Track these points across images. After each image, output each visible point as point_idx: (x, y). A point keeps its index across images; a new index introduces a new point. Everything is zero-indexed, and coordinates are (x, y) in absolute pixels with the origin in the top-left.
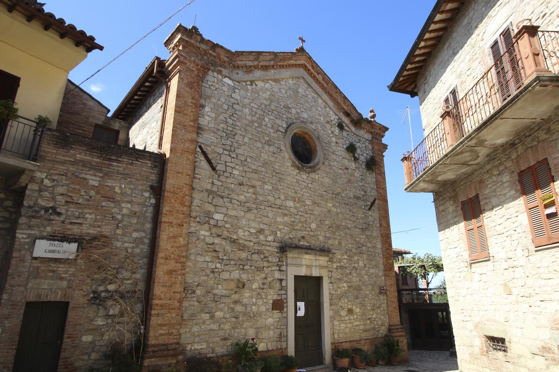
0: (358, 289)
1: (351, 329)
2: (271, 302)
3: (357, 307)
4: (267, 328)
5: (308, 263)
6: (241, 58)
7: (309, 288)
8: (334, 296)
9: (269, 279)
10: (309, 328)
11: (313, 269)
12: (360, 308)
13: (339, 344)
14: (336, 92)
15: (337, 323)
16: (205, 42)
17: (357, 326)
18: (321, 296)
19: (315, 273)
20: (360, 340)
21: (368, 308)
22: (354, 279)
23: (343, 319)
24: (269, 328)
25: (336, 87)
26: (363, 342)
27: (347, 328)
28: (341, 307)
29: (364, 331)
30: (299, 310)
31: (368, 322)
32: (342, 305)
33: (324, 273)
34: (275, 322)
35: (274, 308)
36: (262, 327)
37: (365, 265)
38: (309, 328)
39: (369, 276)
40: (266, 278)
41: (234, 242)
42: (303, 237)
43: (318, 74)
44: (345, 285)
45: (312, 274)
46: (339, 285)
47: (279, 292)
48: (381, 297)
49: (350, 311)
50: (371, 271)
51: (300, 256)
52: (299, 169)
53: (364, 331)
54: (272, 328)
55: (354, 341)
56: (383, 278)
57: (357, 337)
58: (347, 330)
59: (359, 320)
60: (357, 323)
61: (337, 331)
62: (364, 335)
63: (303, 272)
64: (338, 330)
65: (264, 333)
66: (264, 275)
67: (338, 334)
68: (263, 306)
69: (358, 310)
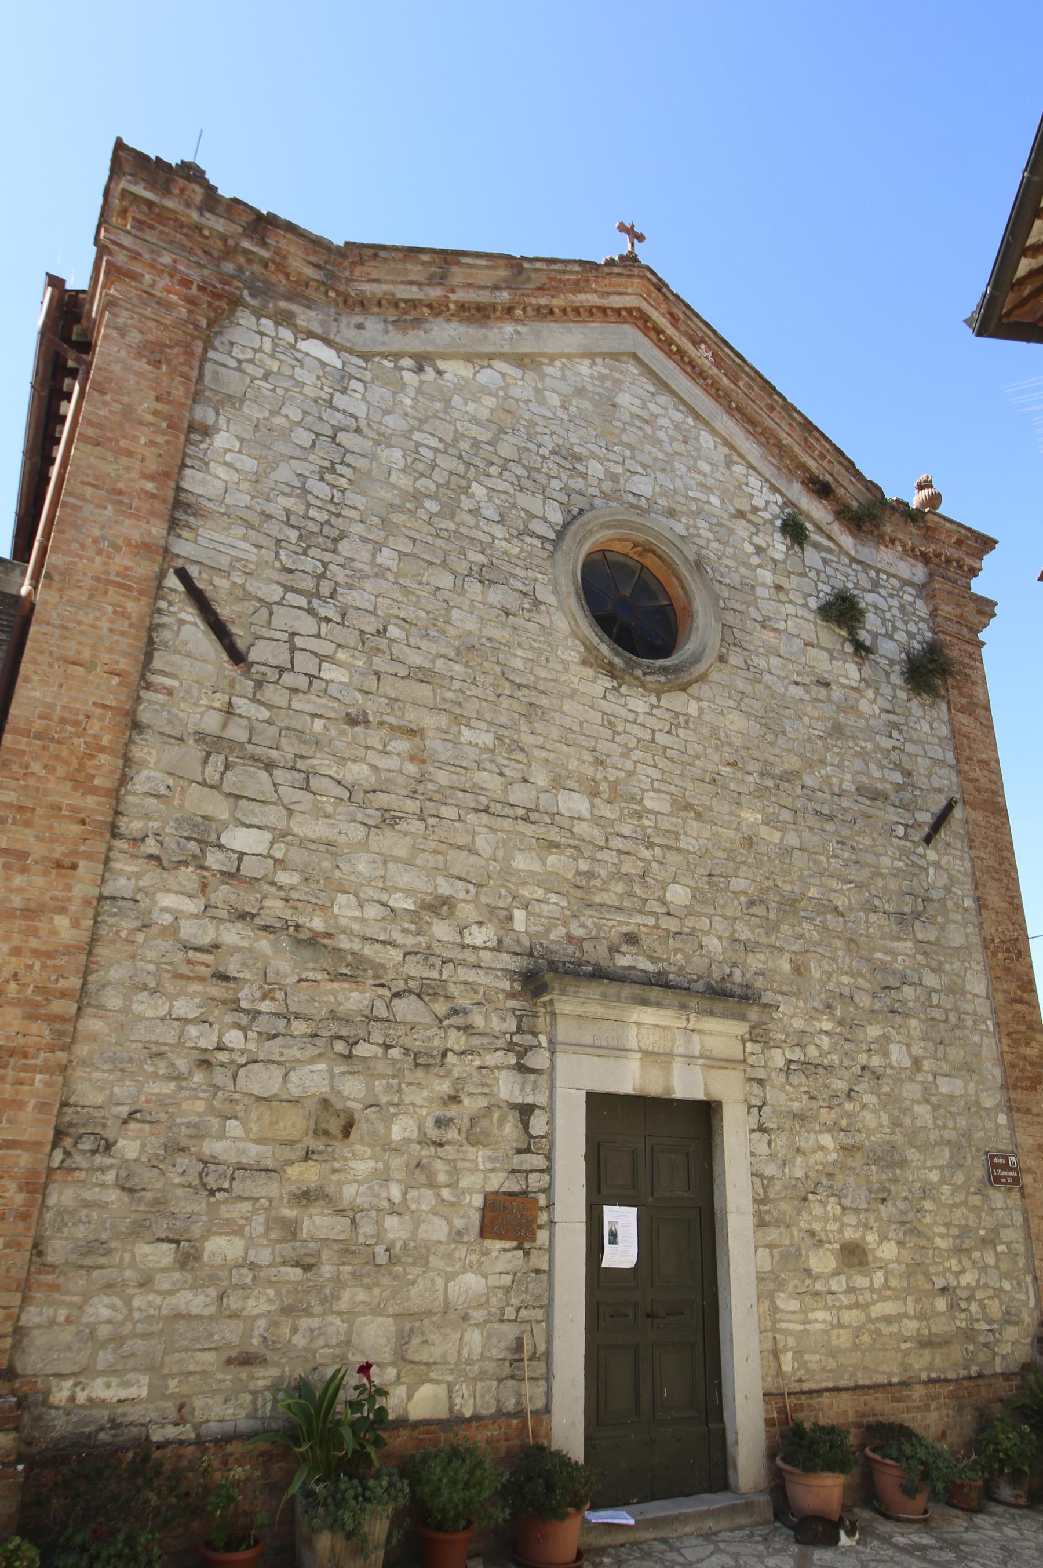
0: (889, 1158)
1: (858, 1331)
2: (478, 1201)
3: (884, 1238)
5: (651, 1041)
6: (371, 269)
7: (659, 1150)
8: (778, 1186)
11: (678, 1067)
12: (901, 1244)
14: (772, 408)
15: (794, 1305)
17: (888, 1319)
19: (686, 1085)
20: (903, 1384)
21: (939, 1242)
22: (869, 1119)
23: (819, 1286)
24: (465, 1318)
25: (769, 388)
27: (840, 1326)
28: (812, 1234)
31: (941, 1304)
32: (817, 1227)
37: (917, 1063)
39: (936, 1108)
43: (695, 344)
44: (826, 1140)
47: (517, 1159)
48: (998, 1197)
49: (853, 1255)
50: (945, 1086)
51: (613, 1014)
54: (478, 1315)
56: (1002, 1119)
57: (888, 1368)
58: (842, 1339)
59: (900, 1296)
61: (791, 1341)
62: (921, 1364)
63: (627, 1078)
64: (800, 1336)
67: (798, 1353)
68: (437, 1217)
69: (888, 1251)
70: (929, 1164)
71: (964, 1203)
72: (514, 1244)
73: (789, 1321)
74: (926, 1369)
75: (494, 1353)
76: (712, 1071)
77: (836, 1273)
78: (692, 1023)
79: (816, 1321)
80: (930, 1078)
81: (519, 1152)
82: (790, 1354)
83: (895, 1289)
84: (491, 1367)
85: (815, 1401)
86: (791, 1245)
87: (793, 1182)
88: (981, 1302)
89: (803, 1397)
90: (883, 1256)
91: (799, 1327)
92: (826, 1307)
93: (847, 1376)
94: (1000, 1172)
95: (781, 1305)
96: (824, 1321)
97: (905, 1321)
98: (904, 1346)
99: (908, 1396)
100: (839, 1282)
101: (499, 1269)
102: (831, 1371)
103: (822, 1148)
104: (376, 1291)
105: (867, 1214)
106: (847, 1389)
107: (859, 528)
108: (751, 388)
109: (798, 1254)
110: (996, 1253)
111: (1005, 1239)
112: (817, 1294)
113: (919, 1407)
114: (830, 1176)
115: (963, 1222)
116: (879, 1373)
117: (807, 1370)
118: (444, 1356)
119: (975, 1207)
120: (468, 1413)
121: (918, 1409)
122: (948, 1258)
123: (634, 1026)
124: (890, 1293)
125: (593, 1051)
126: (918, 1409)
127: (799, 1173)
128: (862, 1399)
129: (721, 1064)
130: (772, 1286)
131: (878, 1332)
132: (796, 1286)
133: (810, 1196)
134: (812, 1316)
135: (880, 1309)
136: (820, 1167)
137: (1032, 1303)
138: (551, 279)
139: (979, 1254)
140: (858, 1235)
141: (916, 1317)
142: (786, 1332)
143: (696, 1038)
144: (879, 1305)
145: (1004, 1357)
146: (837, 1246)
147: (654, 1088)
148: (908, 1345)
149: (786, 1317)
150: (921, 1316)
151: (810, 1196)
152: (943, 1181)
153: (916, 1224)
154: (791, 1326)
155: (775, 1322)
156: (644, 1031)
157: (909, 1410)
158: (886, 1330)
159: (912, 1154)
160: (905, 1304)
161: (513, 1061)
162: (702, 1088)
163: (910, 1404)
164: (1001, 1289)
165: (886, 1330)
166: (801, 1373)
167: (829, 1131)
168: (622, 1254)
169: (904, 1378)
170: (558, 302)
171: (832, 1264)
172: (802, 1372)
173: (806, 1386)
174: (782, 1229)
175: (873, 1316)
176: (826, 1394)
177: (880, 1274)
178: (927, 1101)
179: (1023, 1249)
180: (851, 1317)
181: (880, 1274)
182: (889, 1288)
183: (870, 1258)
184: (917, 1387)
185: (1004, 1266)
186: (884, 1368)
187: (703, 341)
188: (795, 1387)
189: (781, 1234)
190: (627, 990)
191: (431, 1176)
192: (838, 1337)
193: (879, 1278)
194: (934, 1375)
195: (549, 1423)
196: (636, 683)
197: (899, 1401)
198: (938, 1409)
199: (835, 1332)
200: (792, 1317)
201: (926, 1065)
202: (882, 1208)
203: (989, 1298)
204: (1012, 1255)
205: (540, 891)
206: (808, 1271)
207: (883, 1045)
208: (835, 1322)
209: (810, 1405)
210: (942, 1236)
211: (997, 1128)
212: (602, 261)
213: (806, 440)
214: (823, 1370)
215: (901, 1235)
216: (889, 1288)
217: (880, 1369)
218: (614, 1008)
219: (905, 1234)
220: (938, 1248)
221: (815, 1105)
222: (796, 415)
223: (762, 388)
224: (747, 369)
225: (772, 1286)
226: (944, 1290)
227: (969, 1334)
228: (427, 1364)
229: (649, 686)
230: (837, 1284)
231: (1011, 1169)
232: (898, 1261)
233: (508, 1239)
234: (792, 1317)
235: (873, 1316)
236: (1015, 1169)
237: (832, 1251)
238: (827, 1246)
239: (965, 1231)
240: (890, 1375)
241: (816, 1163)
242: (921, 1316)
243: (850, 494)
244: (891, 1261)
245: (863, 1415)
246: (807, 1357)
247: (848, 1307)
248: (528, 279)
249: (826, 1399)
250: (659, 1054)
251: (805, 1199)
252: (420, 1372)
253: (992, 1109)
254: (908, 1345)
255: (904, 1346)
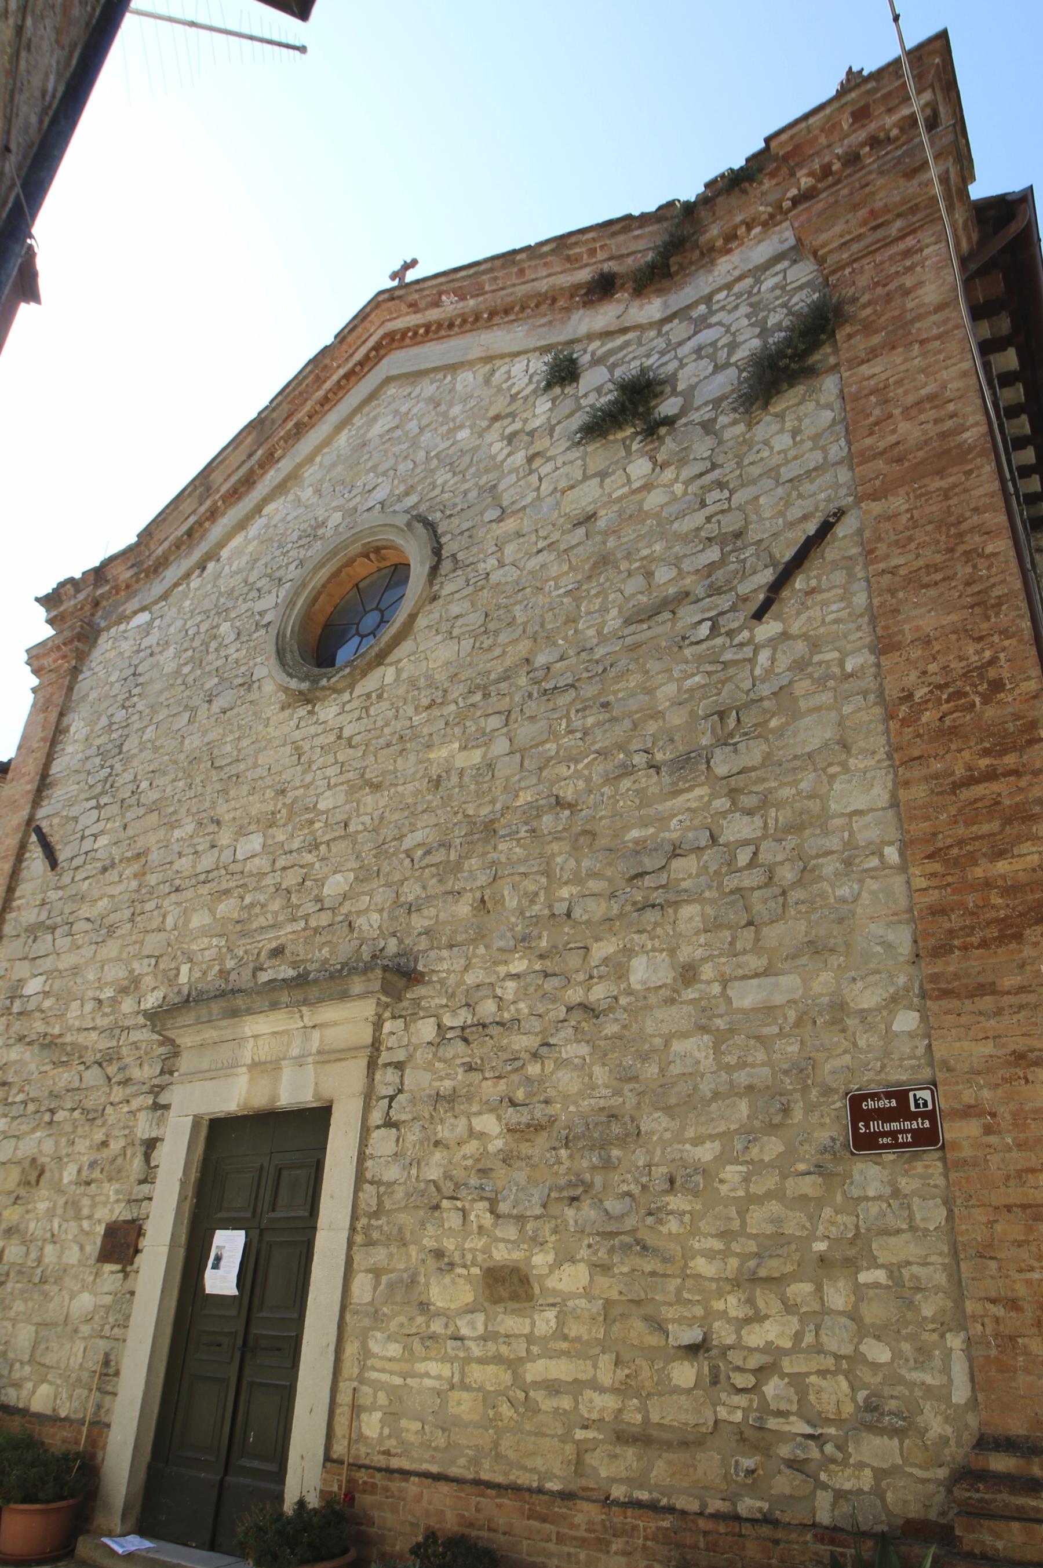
0: (608, 1133)
1: (489, 1400)
2: (101, 1229)
3: (565, 1257)
4: (69, 1328)
5: (265, 1051)
6: (159, 535)
7: (260, 1167)
8: (400, 1193)
9: (115, 1146)
10: (229, 1360)
11: (287, 1072)
12: (602, 1268)
13: (378, 1479)
14: (522, 272)
15: (394, 1349)
16: (82, 585)
17: (553, 1387)
18: (194, 1176)
19: (293, 1091)
20: (567, 1496)
21: (701, 1265)
22: (567, 1081)
23: (437, 1326)
24: (76, 1331)
25: (508, 258)
26: (586, 1514)
27: (464, 1387)
28: (439, 1254)
29: (623, 1437)
30: (216, 1266)
31: (684, 1374)
32: (449, 1244)
33: (344, 1089)
34: (96, 1308)
35: (106, 1255)
36: (55, 1324)
37: (688, 974)
38: (229, 1360)
39: (720, 1039)
40: (104, 1144)
41: (49, 1044)
42: (277, 952)
43: (437, 304)
44: (488, 1123)
45: (274, 1097)
46: (443, 1132)
47: (137, 1188)
48: (870, 1175)
49: (508, 1286)
50: (747, 996)
51: (228, 1034)
52: (308, 701)
53: (623, 1437)
54: (85, 1329)
55: (515, 1489)
56: (906, 1021)
57: (547, 1465)
58: (463, 1405)
59: (579, 1350)
60: (561, 1370)
61: (382, 1398)
62: (613, 1469)
63: (235, 1095)
64: (393, 1392)
65: (54, 1345)
66: (99, 1136)
67: (391, 1416)
68: (76, 1246)
69: (572, 1279)
70: (690, 1133)
71: (777, 1194)
72: (118, 1267)
73: (383, 1371)
74: (629, 1481)
75: (89, 1365)
76: (327, 1067)
77: (470, 1310)
78: (306, 1019)
79: (427, 1375)
80: (716, 989)
81: (141, 1182)
82: (378, 1415)
83: (578, 1339)
84: (85, 1375)
85: (395, 1485)
86: (406, 1270)
87: (422, 1186)
88: (797, 1380)
89: (378, 1475)
90: (559, 1286)
91: (398, 1381)
92: (445, 1359)
93: (462, 1461)
94: (885, 1122)
95: (375, 1347)
96: (439, 1377)
97: (588, 1394)
98: (580, 1434)
99: (564, 1517)
100: (472, 1325)
101: (105, 1290)
102: (436, 1449)
103: (481, 1136)
104: (30, 1304)
105: (538, 1223)
106: (458, 1481)
107: (669, 275)
108: (496, 279)
109: (414, 1281)
110: (857, 1288)
111: (883, 1257)
112: (432, 1337)
113: (584, 1540)
114: (484, 1172)
115: (770, 1229)
116: (525, 1469)
117: (402, 1442)
118: (58, 1362)
119: (804, 1198)
120: (63, 1415)
121: (583, 1543)
122: (720, 1295)
123: (251, 1040)
124: (565, 1345)
125: (201, 1076)
126: (583, 1543)
127: (433, 1173)
128: (474, 1500)
129: (333, 1057)
130: (367, 1322)
131: (531, 1408)
132: (402, 1325)
133: (445, 1204)
134: (420, 1367)
135: (536, 1370)
136: (469, 1162)
137: (960, 1394)
138: (291, 402)
139: (807, 1288)
140: (516, 1255)
141: (614, 1391)
142: (377, 1386)
143: (316, 1034)
144: (541, 1363)
145: (840, 1495)
146: (475, 1271)
147: (259, 1101)
148: (590, 1434)
149: (379, 1364)
150: (623, 1390)
151: (445, 1204)
152: (723, 1159)
153: (644, 1234)
154: (384, 1377)
155: (363, 1369)
156: (260, 1042)
157: (560, 1539)
158: (547, 1404)
159: (655, 1123)
160: (595, 1366)
161: (151, 1102)
162: (313, 1086)
163: (565, 1530)
164: (857, 1358)
165: (547, 1404)
166: (391, 1444)
167: (491, 1111)
168: (221, 1280)
169: (573, 1487)
170: (301, 415)
171: (466, 1295)
172: (393, 1442)
173: (395, 1463)
174: (393, 1249)
175: (529, 1378)
176: (414, 1479)
177: (551, 1314)
178: (704, 1029)
179: (941, 1278)
180: (488, 1376)
181: (551, 1314)
182: (565, 1338)
183: (537, 1290)
184: (585, 1506)
185: (873, 1313)
186: (538, 1462)
187: (440, 294)
188: (380, 1461)
189: (391, 1256)
190: (216, 1007)
191: (78, 1210)
192: (459, 1403)
193: (546, 1321)
194: (644, 1496)
195: (107, 1437)
196: (328, 693)
197: (544, 1519)
198: (625, 1553)
199: (455, 1395)
200: (388, 1366)
201: (707, 971)
202: (570, 1213)
203: (822, 1373)
204: (902, 1290)
205: (206, 940)
206: (424, 1307)
207: (617, 968)
208: (456, 1379)
209: (386, 1489)
210: (710, 1255)
211: (892, 1041)
212: (763, 145)
213: (568, 259)
214: (426, 1445)
215: (602, 1254)
216: (565, 1338)
217: (529, 1463)
218: (226, 1028)
219: (611, 1251)
220: (698, 1276)
221: (476, 1077)
222: (545, 249)
223: (504, 266)
224: (483, 267)
225: (367, 1322)
226: (693, 1350)
227: (754, 1437)
228: (48, 1367)
229: (340, 686)
230: (470, 1326)
231: (913, 1117)
232: (587, 1294)
233: (117, 1263)
234: (388, 1366)
235: (529, 1378)
236: (924, 1115)
237: (468, 1278)
238: (460, 1270)
239: (776, 1242)
240: (545, 1476)
241: (464, 1157)
242: (623, 1390)
243: (641, 250)
244: (573, 1296)
245: (471, 1525)
246: (404, 1423)
247: (480, 1361)
248: (273, 422)
249: (413, 1486)
250: (266, 1063)
251: (437, 1207)
252: (43, 1372)
253: (878, 1009)
254: (590, 1434)
255: (580, 1434)
